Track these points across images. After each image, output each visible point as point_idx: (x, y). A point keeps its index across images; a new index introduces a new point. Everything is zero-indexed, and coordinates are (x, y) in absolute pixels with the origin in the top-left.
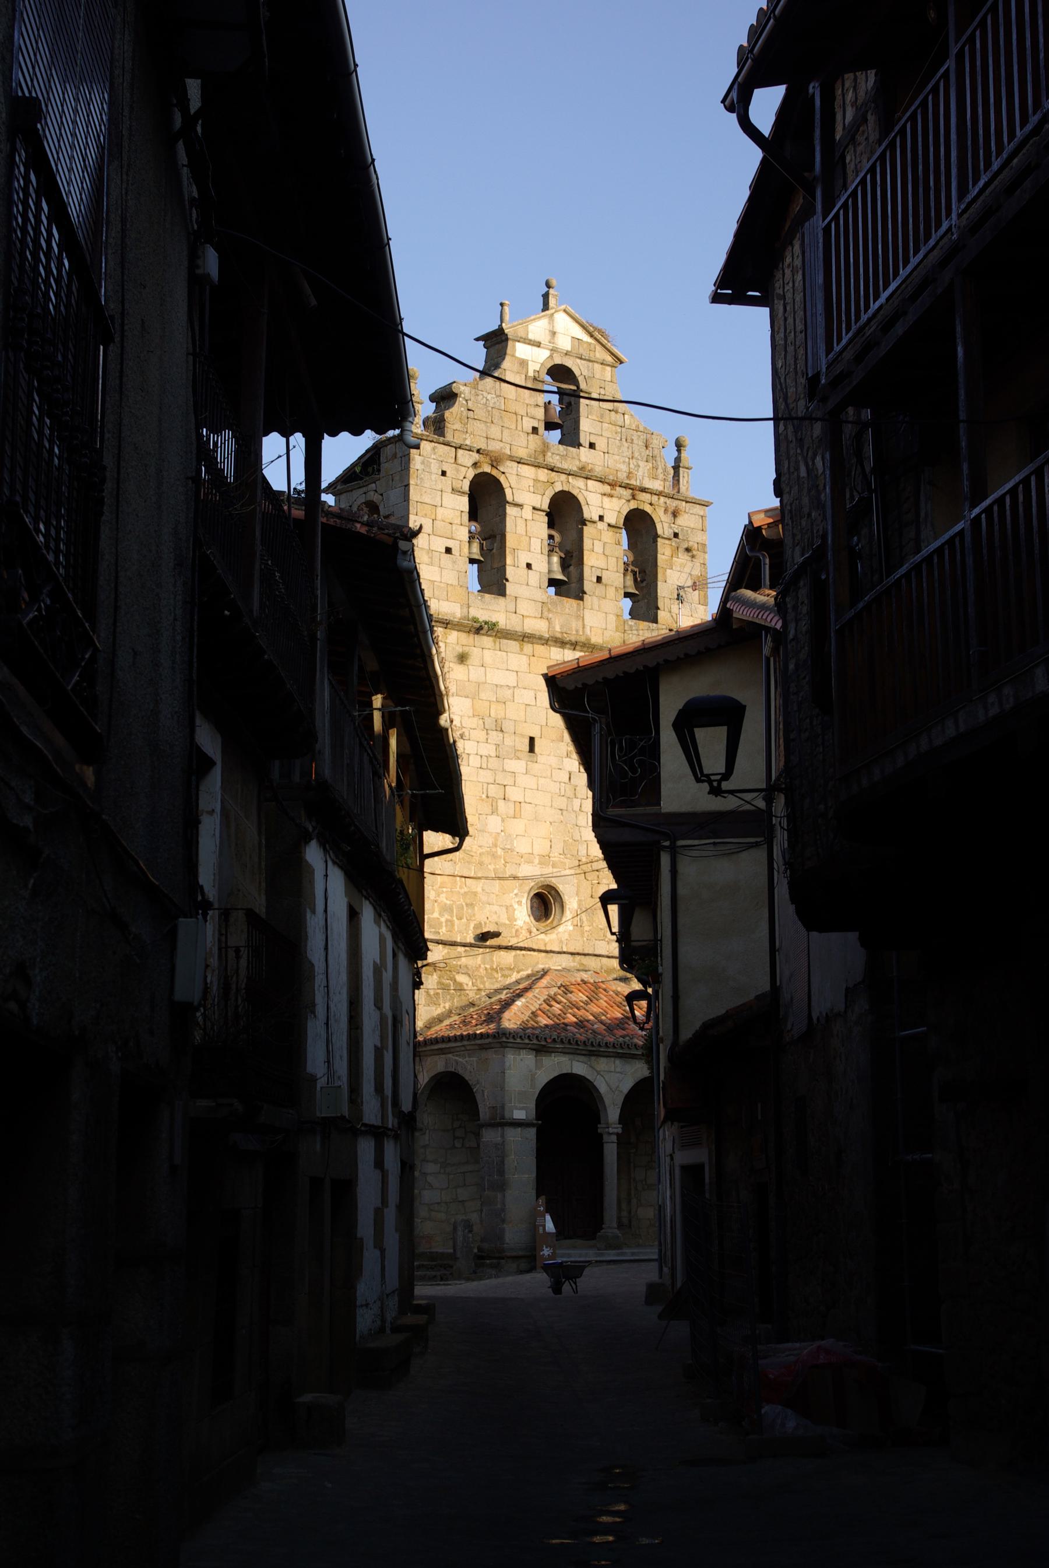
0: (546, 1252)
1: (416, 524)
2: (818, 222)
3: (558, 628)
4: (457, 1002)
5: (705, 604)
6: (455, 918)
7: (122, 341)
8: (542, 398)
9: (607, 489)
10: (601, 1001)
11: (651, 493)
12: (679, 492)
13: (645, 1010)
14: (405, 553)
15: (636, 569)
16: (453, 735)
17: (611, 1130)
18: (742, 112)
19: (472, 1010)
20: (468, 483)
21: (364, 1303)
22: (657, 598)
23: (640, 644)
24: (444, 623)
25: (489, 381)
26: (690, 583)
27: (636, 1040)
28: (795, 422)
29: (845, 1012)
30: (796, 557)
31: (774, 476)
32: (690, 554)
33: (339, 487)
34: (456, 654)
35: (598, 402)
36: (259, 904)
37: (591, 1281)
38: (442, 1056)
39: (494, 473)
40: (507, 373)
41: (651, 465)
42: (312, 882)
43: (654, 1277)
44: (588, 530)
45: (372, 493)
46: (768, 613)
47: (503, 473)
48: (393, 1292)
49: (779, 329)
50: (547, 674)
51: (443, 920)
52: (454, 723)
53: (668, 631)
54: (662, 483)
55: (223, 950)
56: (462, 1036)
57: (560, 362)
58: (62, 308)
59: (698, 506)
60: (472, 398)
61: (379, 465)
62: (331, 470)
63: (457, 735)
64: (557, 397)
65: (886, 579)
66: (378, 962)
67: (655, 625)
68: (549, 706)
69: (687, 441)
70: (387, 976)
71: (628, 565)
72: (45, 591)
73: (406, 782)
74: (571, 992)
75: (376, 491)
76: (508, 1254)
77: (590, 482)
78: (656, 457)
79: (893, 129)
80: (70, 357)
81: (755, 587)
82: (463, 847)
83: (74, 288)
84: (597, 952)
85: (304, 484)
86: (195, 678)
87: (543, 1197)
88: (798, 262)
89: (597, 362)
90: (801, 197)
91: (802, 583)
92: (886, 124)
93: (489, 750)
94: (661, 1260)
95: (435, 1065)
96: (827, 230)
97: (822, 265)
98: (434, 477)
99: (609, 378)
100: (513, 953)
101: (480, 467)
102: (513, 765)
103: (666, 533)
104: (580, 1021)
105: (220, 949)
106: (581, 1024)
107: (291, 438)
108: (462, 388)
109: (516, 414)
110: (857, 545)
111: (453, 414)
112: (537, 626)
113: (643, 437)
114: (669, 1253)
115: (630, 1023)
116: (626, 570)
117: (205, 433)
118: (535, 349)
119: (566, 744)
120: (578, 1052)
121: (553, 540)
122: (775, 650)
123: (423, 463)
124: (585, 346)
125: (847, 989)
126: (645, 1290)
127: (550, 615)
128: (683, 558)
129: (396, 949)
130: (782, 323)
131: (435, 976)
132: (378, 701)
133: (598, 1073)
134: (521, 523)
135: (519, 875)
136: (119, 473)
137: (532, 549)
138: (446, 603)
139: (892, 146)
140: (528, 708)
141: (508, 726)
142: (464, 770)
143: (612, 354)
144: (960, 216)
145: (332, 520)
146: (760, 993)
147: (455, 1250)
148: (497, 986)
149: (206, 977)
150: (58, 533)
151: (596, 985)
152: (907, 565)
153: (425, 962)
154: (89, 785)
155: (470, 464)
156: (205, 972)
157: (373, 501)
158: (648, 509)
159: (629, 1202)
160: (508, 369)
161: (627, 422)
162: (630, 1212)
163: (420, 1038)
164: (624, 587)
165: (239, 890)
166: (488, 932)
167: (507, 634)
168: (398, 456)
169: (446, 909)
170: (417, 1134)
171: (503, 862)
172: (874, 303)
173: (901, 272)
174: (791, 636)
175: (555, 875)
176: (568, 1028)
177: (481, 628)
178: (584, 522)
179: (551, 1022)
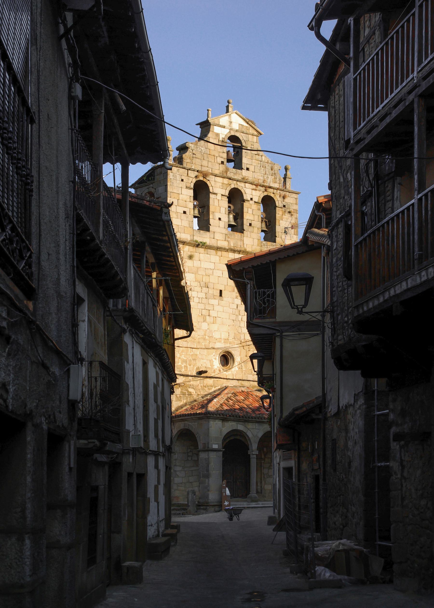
0: (226, 503)
1: (170, 201)
2: (351, 76)
3: (232, 245)
4: (189, 400)
5: (297, 235)
6: (188, 365)
7: (39, 123)
8: (225, 150)
9: (254, 187)
10: (250, 399)
11: (274, 189)
12: (286, 188)
13: (269, 403)
14: (166, 213)
15: (267, 220)
16: (187, 289)
17: (254, 453)
18: (317, 31)
19: (195, 403)
20: (193, 185)
21: (150, 524)
22: (276, 233)
23: (268, 251)
24: (182, 243)
25: (202, 142)
26: (290, 226)
27: (264, 416)
28: (339, 159)
29: (354, 404)
30: (337, 215)
31: (329, 181)
32: (290, 214)
33: (136, 186)
34: (188, 255)
35: (250, 151)
36: (105, 359)
37: (245, 516)
38: (182, 422)
39: (205, 180)
40: (210, 138)
41: (274, 177)
42: (127, 350)
43: (272, 514)
44: (246, 204)
45: (151, 188)
46: (324, 238)
47: (209, 180)
48: (163, 520)
49: (332, 120)
50: (227, 264)
51: (183, 366)
52: (187, 284)
53: (280, 246)
54: (279, 184)
55: (90, 378)
56: (191, 414)
57: (233, 134)
58: (11, 108)
59: (294, 194)
60: (195, 149)
61: (154, 177)
62: (133, 179)
63: (188, 289)
64: (232, 148)
65: (378, 224)
66: (156, 383)
67: (274, 243)
68: (228, 277)
69: (289, 167)
70: (160, 389)
71: (263, 218)
72: (8, 228)
73: (167, 308)
74: (237, 396)
75: (153, 187)
76: (210, 504)
77: (246, 184)
78: (276, 174)
79: (387, 37)
80: (16, 129)
81: (319, 228)
82: (191, 336)
83: (17, 100)
84: (248, 379)
85: (121, 184)
86: (75, 265)
87: (225, 481)
88: (342, 93)
89: (250, 134)
90: (344, 66)
91: (340, 226)
92: (385, 34)
93: (202, 295)
94: (274, 507)
95: (179, 427)
96: (355, 79)
97: (353, 94)
98: (178, 182)
99: (255, 141)
100: (213, 379)
101: (198, 178)
102: (212, 301)
103: (280, 205)
104: (241, 408)
105: (88, 378)
106: (241, 409)
107: (115, 165)
108: (190, 145)
109: (214, 156)
110: (365, 210)
111: (186, 156)
112: (224, 244)
113: (270, 165)
114: (277, 504)
115: (262, 408)
116: (262, 221)
117: (77, 162)
118: (222, 128)
119: (236, 293)
120: (240, 420)
121: (230, 208)
122: (327, 254)
123: (173, 176)
124: (245, 127)
125: (355, 394)
126: (267, 519)
127: (229, 240)
128: (287, 216)
129: (163, 378)
130: (334, 118)
131: (180, 389)
132: (154, 275)
133: (248, 429)
134: (216, 201)
135: (215, 347)
136: (39, 178)
137: (221, 212)
138: (184, 234)
139: (387, 44)
140: (219, 278)
141: (211, 285)
142: (192, 303)
143: (257, 131)
144: (418, 73)
145: (134, 199)
146: (317, 396)
147: (188, 503)
148: (206, 393)
149: (83, 389)
150: (13, 203)
151: (248, 393)
152: (387, 218)
153: (175, 383)
154: (31, 309)
155: (194, 176)
156: (82, 387)
157: (151, 192)
158: (272, 195)
159: (261, 483)
160: (211, 137)
161: (263, 159)
162: (261, 487)
163: (173, 415)
164: (261, 228)
165: (96, 353)
166: (202, 371)
167: (210, 247)
168: (162, 173)
169: (184, 361)
170: (172, 454)
171: (208, 342)
172: (376, 109)
173: (389, 96)
174: (334, 248)
175: (230, 347)
176: (236, 410)
177: (199, 245)
178: (244, 201)
179: (229, 408)
